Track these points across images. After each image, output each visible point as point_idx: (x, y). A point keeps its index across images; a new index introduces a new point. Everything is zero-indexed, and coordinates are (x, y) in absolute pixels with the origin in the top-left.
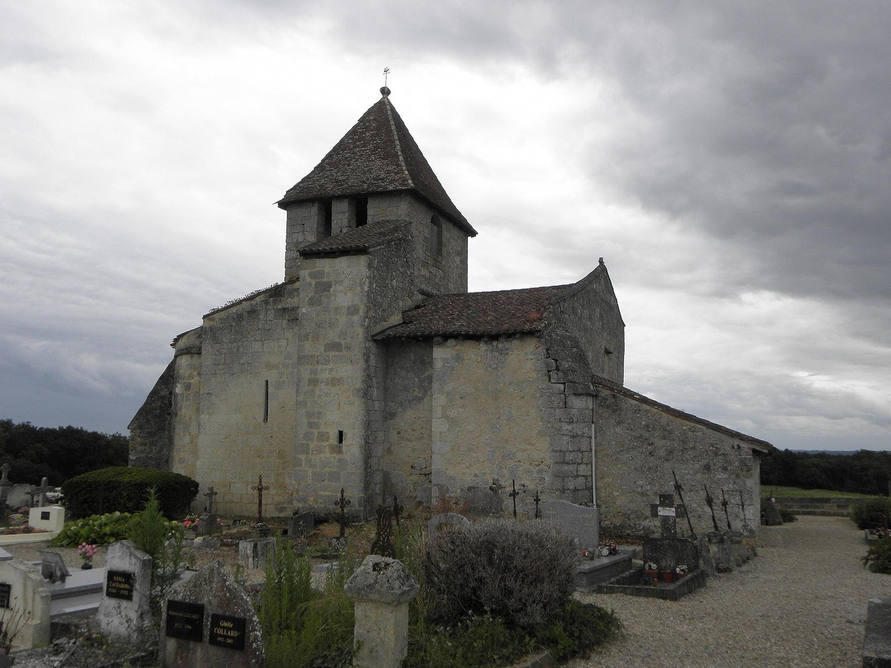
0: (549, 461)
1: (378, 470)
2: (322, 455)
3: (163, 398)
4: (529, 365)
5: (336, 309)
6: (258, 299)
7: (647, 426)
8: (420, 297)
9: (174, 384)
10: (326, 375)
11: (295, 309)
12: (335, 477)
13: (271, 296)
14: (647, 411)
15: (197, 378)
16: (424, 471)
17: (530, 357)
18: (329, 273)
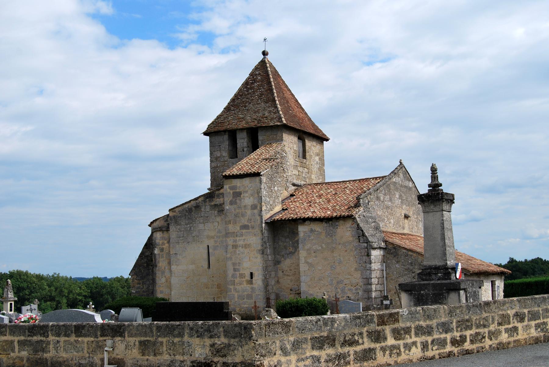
0: (361, 284)
1: (272, 292)
2: (242, 286)
3: (147, 256)
4: (348, 234)
5: (245, 206)
6: (200, 200)
7: (411, 263)
8: (294, 188)
9: (153, 249)
10: (241, 243)
11: (222, 205)
12: (249, 297)
13: (207, 198)
14: (411, 255)
15: (167, 245)
16: (297, 292)
17: (349, 229)
18: (239, 187)
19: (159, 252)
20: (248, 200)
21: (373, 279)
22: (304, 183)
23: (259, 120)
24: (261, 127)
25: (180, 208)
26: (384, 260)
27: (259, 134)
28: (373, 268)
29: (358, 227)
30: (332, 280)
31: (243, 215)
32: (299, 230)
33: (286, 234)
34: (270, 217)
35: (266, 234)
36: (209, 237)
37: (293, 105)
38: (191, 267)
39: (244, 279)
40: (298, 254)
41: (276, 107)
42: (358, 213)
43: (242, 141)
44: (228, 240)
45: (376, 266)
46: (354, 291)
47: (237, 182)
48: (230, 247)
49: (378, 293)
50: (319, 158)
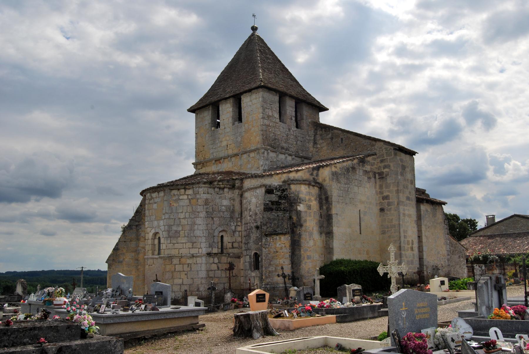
19: (306, 209)
36: (362, 202)
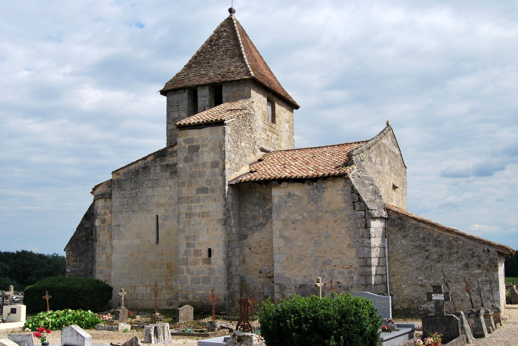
0: (356, 265)
1: (236, 275)
2: (197, 266)
3: (87, 229)
5: (204, 164)
6: (149, 159)
7: (424, 238)
9: (94, 221)
10: (197, 210)
11: (175, 165)
12: (206, 280)
13: (158, 157)
14: (424, 228)
15: (109, 215)
16: (268, 275)
17: (340, 192)
18: (197, 139)
19: (100, 224)
20: (207, 156)
21: (372, 259)
22: (274, 150)
23: (224, 75)
24: (226, 82)
25: (125, 169)
26: (386, 234)
27: (223, 91)
28: (372, 244)
29: (353, 190)
30: (316, 260)
31: (200, 176)
32: (273, 194)
33: (255, 201)
34: (235, 179)
35: (230, 200)
36: (158, 205)
37: (261, 66)
38: (136, 242)
39: (200, 258)
40: (271, 225)
41: (244, 62)
42: (352, 172)
43: (204, 96)
44: (181, 206)
45: (376, 241)
46: (346, 275)
47: (194, 134)
48: (183, 216)
49: (379, 278)
50: (289, 126)
